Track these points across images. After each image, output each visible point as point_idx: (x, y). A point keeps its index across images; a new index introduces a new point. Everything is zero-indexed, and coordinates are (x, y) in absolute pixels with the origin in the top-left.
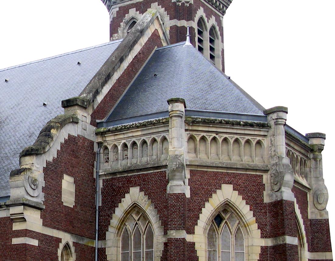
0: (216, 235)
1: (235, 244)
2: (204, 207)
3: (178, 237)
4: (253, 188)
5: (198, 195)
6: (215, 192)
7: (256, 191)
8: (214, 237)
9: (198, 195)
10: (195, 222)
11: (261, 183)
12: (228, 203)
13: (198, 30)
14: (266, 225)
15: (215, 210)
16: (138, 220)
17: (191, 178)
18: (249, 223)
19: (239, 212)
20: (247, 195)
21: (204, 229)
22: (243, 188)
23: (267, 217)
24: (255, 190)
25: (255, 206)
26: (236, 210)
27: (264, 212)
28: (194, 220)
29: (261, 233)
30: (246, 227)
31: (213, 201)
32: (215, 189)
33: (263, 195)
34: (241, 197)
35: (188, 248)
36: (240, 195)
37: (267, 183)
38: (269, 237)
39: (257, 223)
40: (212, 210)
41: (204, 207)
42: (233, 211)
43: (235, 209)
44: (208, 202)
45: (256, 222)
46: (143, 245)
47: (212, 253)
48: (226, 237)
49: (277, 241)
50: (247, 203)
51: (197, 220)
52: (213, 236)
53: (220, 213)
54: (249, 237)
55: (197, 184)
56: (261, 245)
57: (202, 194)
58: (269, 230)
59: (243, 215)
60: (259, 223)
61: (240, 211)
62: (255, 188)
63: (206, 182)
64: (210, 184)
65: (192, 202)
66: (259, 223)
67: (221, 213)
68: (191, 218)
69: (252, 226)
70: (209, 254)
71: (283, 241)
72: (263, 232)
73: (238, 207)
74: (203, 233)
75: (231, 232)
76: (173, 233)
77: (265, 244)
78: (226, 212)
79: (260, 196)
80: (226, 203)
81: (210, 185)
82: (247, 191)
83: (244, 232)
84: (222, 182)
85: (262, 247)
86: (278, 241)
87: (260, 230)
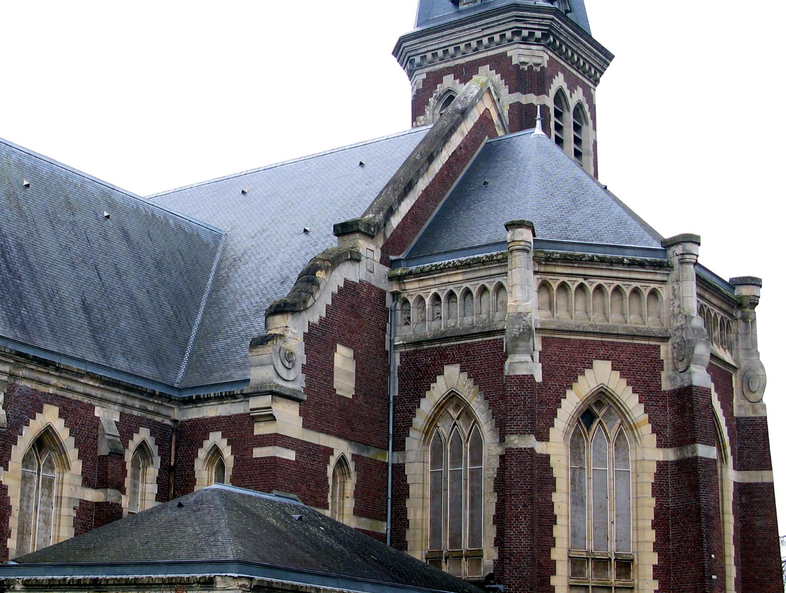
0: (584, 442)
1: (616, 458)
2: (565, 398)
3: (523, 446)
6: (583, 374)
8: (581, 445)
10: (550, 421)
11: (657, 358)
12: (603, 391)
13: (555, 109)
14: (665, 426)
16: (458, 419)
18: (638, 424)
19: (622, 405)
20: (634, 378)
24: (647, 370)
25: (647, 396)
27: (662, 406)
29: (657, 440)
30: (632, 430)
34: (625, 380)
37: (667, 358)
38: (671, 446)
41: (565, 398)
42: (611, 404)
43: (615, 400)
44: (572, 389)
47: (578, 472)
48: (601, 446)
50: (634, 392)
51: (553, 419)
60: (653, 422)
66: (653, 422)
68: (543, 416)
70: (573, 474)
73: (619, 397)
75: (608, 438)
76: (514, 440)
77: (663, 458)
79: (656, 379)
81: (575, 362)
85: (658, 463)
87: (655, 435)
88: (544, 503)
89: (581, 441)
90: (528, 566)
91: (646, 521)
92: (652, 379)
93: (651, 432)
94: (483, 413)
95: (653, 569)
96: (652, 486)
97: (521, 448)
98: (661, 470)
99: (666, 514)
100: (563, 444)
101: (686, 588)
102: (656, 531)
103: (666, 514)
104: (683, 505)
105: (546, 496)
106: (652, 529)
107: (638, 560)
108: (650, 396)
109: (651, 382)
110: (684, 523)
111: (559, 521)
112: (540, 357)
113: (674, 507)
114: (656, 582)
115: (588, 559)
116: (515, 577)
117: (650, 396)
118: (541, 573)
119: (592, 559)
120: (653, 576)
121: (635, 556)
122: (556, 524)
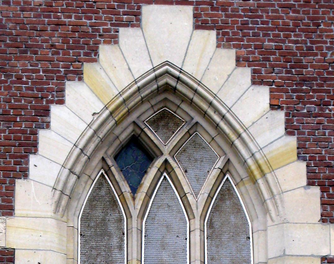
0: (121, 220)
5: (36, 53)
6: (113, 39)
8: (112, 227)
9: (36, 53)
10: (16, 163)
12: (173, 83)
15: (111, 113)
18: (268, 162)
19: (223, 117)
20: (256, 47)
21: (58, 193)
22: (240, 16)
25: (294, 91)
26: (211, 112)
28: (11, 157)
29: (323, 204)
30: (254, 181)
31: (103, 74)
32: (112, 25)
34: (232, 53)
36: (225, 47)
39: (304, 159)
41: (61, 102)
42: (197, 118)
43: (204, 106)
44: (80, 79)
48: (168, 227)
50: (257, 80)
51: (27, 157)
53: (139, 132)
55: (31, 10)
57: (53, 46)
59: (241, 131)
60: (312, 158)
61: (224, 111)
62: (295, 19)
64: (89, 6)
65: (6, 82)
66: (312, 158)
67: (142, 130)
69: (277, 172)
73: (215, 96)
74: (53, 207)
75: (187, 206)
79: (321, 49)
80: (161, 82)
82: (259, 29)
83: (250, 206)
87: (316, 190)
89: (113, 216)
92: (310, 49)
93: (304, 182)
108: (302, 91)
109: (305, 55)
117: (302, 91)
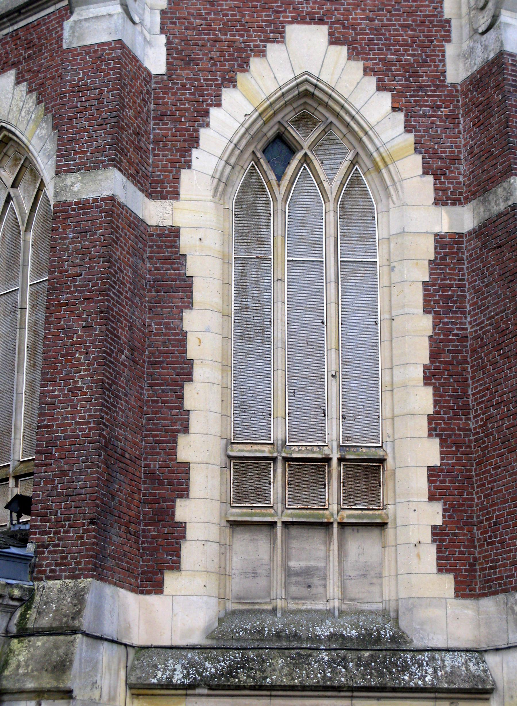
0: (268, 203)
1: (343, 235)
2: (219, 105)
3: (91, 196)
4: (407, 35)
7: (418, 46)
8: (261, 209)
9: (197, 64)
11: (435, 16)
12: (311, 89)
14: (455, 160)
16: (14, 185)
17: (170, 9)
18: (390, 155)
19: (353, 118)
21: (216, 180)
22: (367, 34)
23: (459, 132)
24: (414, 42)
25: (411, 96)
26: (342, 113)
27: (447, 117)
28: (177, 151)
29: (436, 190)
30: (379, 171)
31: (253, 82)
33: (443, 56)
34: (360, 65)
35: (151, 247)
36: (354, 59)
37: (460, 17)
38: (467, 200)
40: (246, 115)
41: (219, 105)
42: (332, 119)
43: (337, 109)
44: (235, 86)
45: (415, 151)
46: (25, 265)
47: (252, 269)
48: (308, 209)
49: (490, 204)
50: (381, 87)
52: (255, 207)
53: (283, 130)
54: (392, 205)
55: (194, 29)
56: (437, 231)
57: (211, 59)
58: (465, 176)
59: (368, 129)
60: (427, 152)
61: (353, 113)
63: (228, 20)
65: (173, 88)
66: (427, 152)
67: (286, 129)
68: (165, 145)
69: (398, 163)
70: (242, 273)
71: (507, 199)
72: (442, 183)
73: (346, 100)
74: (212, 193)
75: (323, 191)
76: (73, 184)
77: (450, 227)
78: (306, 125)
79: (434, 61)
80: (302, 89)
81: (244, 29)
84: (287, 17)
85: (439, 238)
86: (493, 204)
87: (430, 179)
88: (165, 335)
89: (262, 200)
90: (87, 467)
91: (412, 368)
94: (49, 157)
95: (429, 476)
96: (425, 290)
97: (87, 201)
98: (446, 254)
99: (460, 352)
100: (211, 205)
101: (502, 515)
102: (435, 390)
103: (460, 352)
104: (491, 324)
105: (169, 318)
106: (426, 384)
107: (394, 458)
108: (418, 96)
110: (494, 364)
111: (198, 372)
112: (162, 23)
113: (476, 331)
114: (438, 507)
115: (274, 459)
116: (59, 494)
117: (418, 96)
118: (154, 495)
119: (286, 460)
120: (430, 492)
121: (389, 450)
122: (191, 380)
